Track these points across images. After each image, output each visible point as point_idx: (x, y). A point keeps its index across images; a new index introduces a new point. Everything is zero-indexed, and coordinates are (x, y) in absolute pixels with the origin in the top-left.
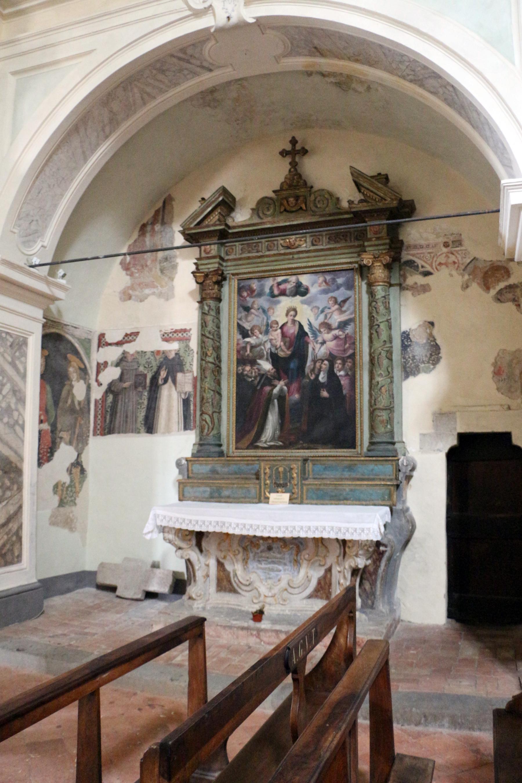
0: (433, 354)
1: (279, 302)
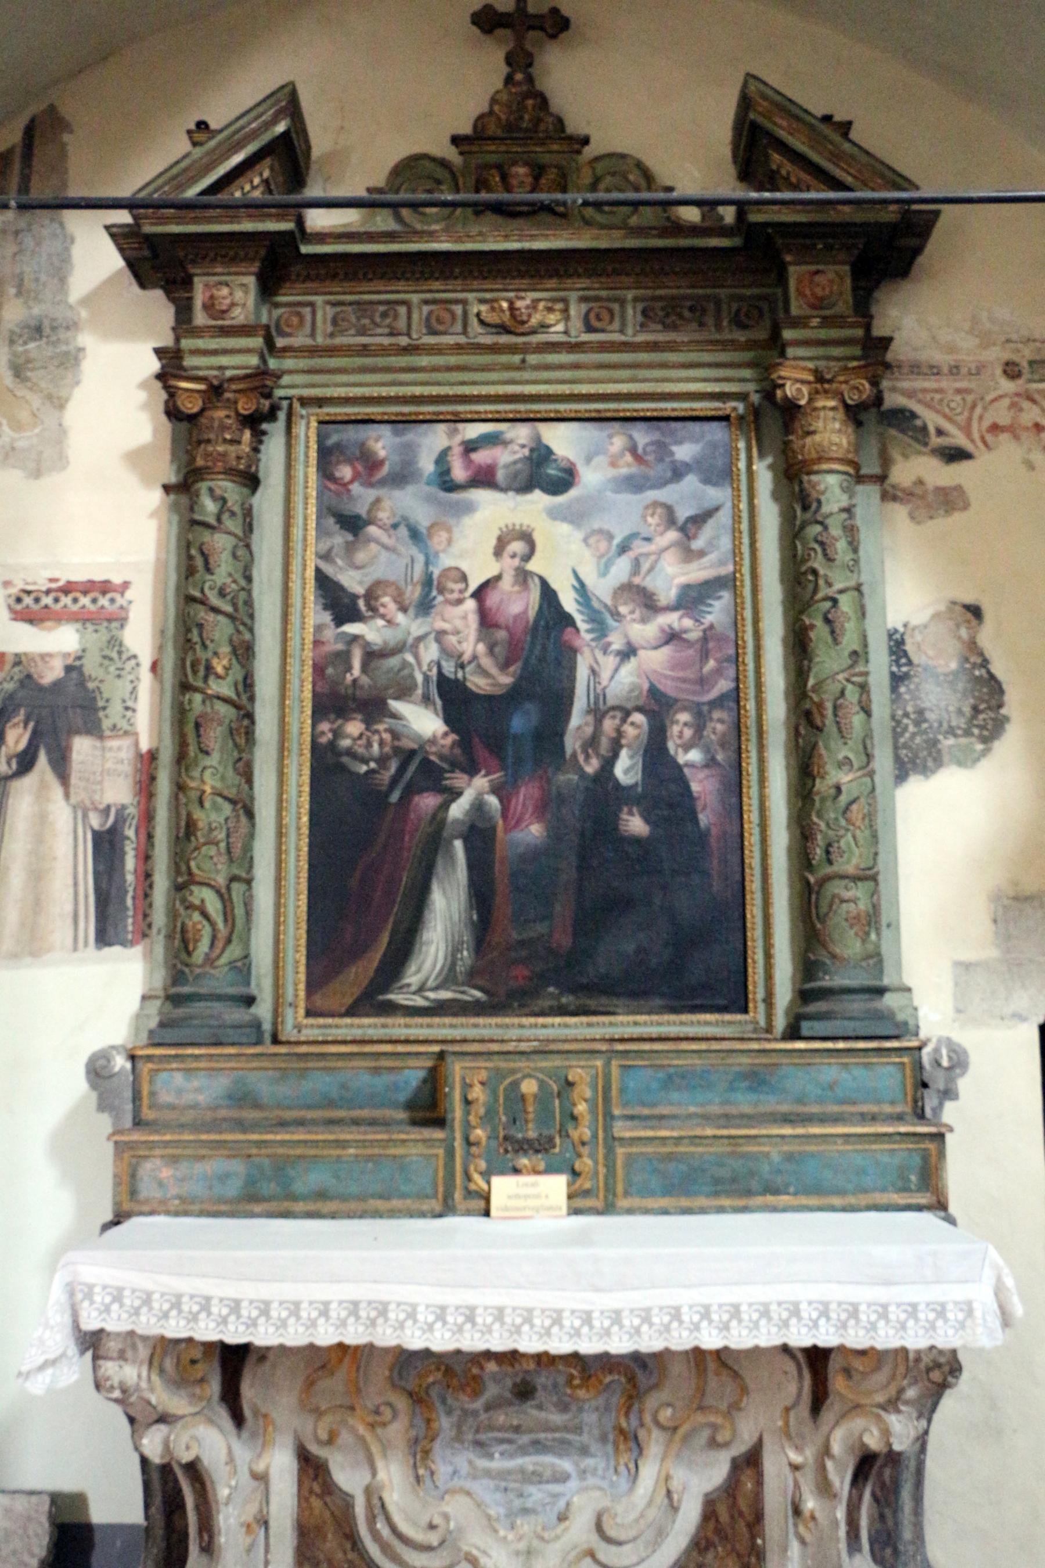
0: (982, 706)
1: (469, 508)
